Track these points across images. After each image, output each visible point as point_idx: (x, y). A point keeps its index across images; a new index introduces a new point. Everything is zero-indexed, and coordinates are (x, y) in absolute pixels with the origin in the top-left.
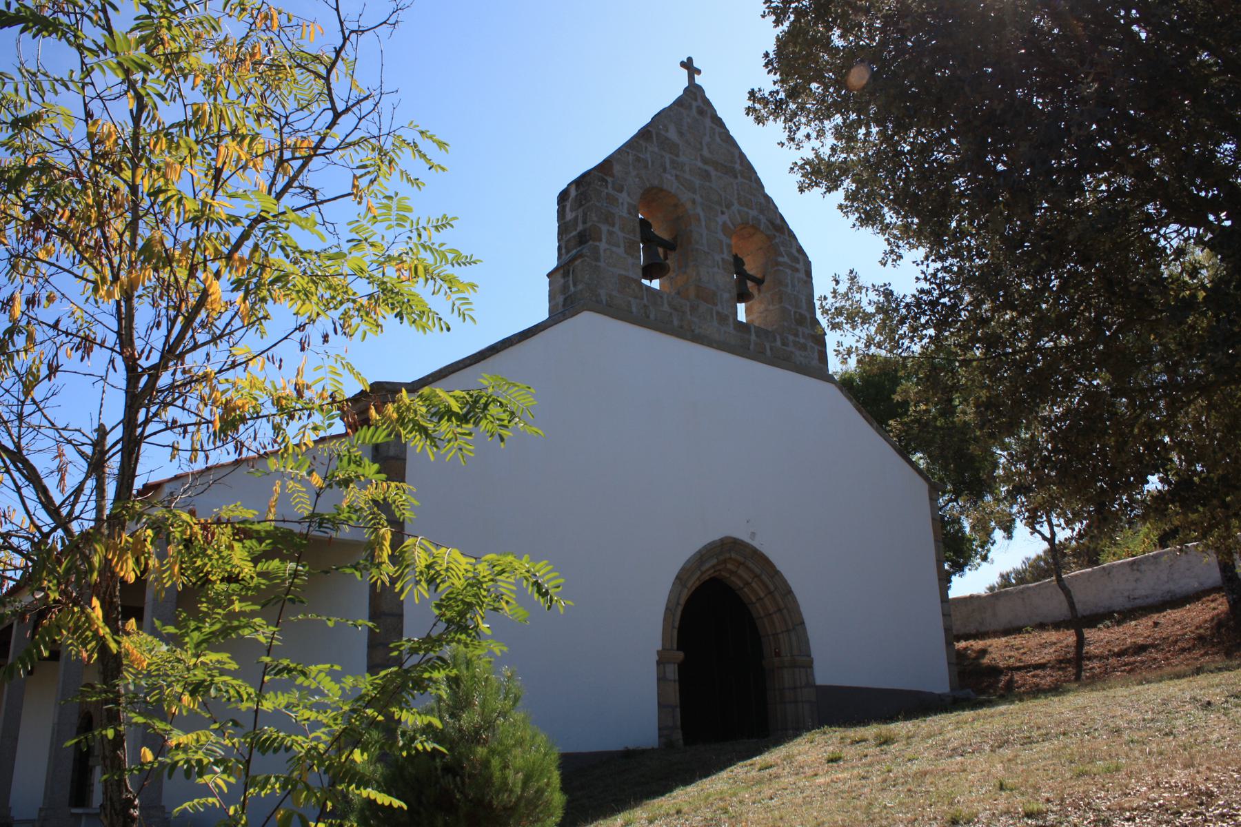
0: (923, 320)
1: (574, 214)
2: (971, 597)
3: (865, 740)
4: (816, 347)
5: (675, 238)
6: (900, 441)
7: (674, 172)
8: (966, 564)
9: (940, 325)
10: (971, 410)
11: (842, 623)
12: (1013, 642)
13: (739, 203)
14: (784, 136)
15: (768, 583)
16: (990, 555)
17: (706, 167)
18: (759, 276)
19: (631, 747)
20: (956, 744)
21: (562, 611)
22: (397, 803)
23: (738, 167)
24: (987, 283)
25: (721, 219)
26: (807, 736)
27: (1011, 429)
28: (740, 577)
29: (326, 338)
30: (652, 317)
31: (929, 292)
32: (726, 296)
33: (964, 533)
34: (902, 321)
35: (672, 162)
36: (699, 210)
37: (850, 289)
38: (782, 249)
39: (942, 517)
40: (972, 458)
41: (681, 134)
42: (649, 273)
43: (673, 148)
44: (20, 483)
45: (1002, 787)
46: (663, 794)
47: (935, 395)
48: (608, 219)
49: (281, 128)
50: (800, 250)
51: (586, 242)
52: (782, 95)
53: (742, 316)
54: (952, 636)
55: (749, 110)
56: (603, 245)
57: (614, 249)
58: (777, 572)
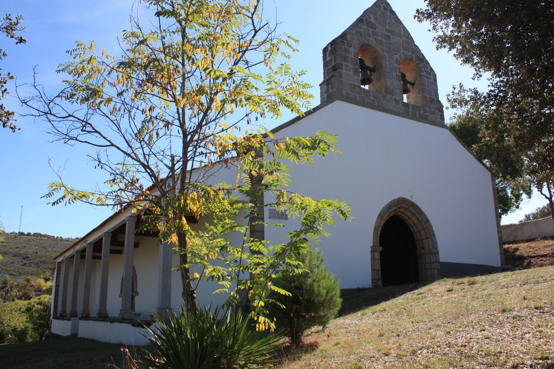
0: (491, 103)
1: (330, 58)
2: (511, 225)
3: (463, 283)
4: (439, 113)
5: (375, 66)
6: (477, 154)
7: (374, 37)
8: (509, 210)
9: (499, 105)
10: (512, 140)
11: (451, 233)
12: (531, 245)
13: (403, 49)
14: (431, 27)
15: (419, 217)
16: (520, 206)
17: (388, 34)
18: (413, 82)
19: (360, 287)
20: (504, 283)
21: (350, 221)
22: (288, 293)
23: (402, 33)
24: (520, 87)
25: (395, 57)
26: (437, 282)
27: (530, 147)
28: (407, 215)
29: (257, 119)
30: (366, 102)
31: (493, 91)
32: (398, 91)
33: (507, 196)
34: (482, 104)
35: (373, 32)
36: (385, 53)
37: (460, 91)
38: (423, 69)
39: (498, 188)
40: (512, 162)
41: (376, 19)
42: (364, 82)
43: (373, 26)
44: (189, 174)
45: (525, 299)
46: (376, 305)
47: (496, 134)
48: (345, 59)
49: (240, 40)
50: (431, 69)
51: (336, 70)
52: (431, 11)
53: (405, 100)
54: (502, 243)
55: (415, 16)
56: (343, 71)
57: (349, 73)
58: (422, 213)
